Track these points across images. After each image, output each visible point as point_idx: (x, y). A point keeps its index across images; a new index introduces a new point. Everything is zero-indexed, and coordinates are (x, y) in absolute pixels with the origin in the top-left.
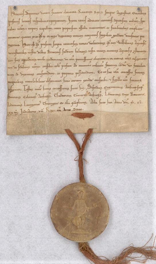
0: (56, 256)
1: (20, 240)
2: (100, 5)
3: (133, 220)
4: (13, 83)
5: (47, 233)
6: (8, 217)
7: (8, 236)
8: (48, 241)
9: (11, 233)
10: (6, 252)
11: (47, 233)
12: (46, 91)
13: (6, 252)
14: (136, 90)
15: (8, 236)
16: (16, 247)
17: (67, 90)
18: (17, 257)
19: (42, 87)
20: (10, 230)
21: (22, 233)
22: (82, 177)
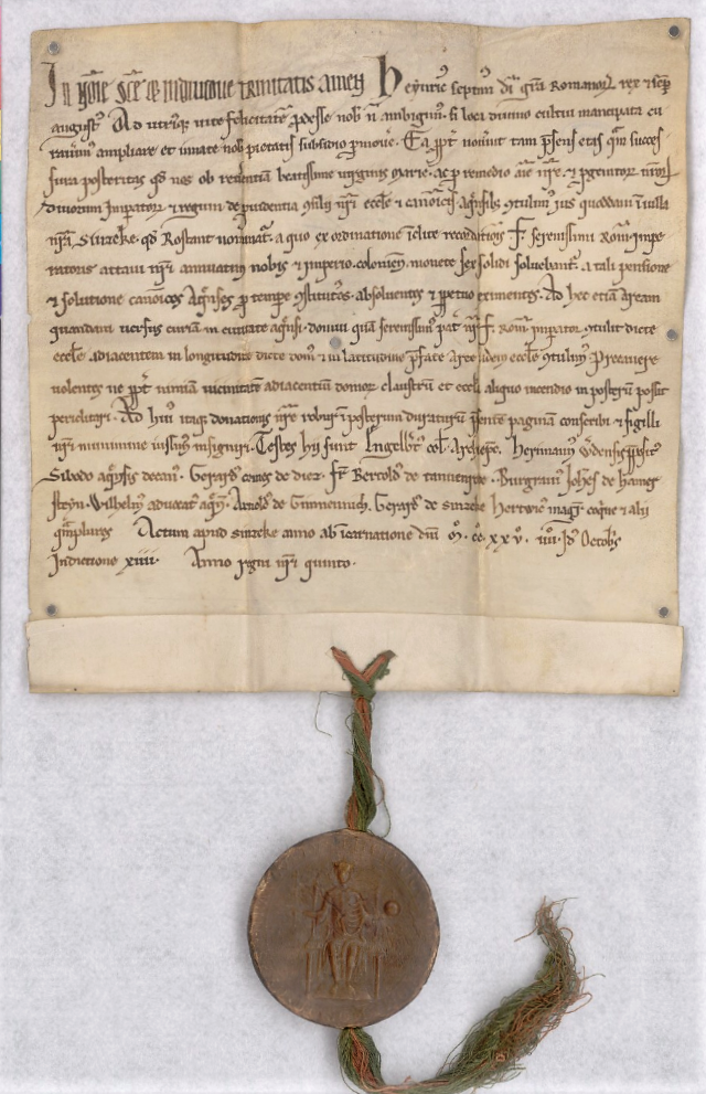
0: (192, 843)
1: (76, 793)
2: (238, 25)
3: (444, 724)
4: (325, 268)
5: (162, 770)
6: (35, 717)
7: (34, 778)
8: (167, 794)
9: (46, 770)
10: (27, 831)
11: (162, 770)
12: (565, 163)
13: (27, 831)
14: (475, 212)
15: (34, 778)
16: (60, 814)
17: (614, 198)
18: (63, 846)
19: (369, 500)
20: (40, 759)
21: (79, 768)
22: (363, 795)
